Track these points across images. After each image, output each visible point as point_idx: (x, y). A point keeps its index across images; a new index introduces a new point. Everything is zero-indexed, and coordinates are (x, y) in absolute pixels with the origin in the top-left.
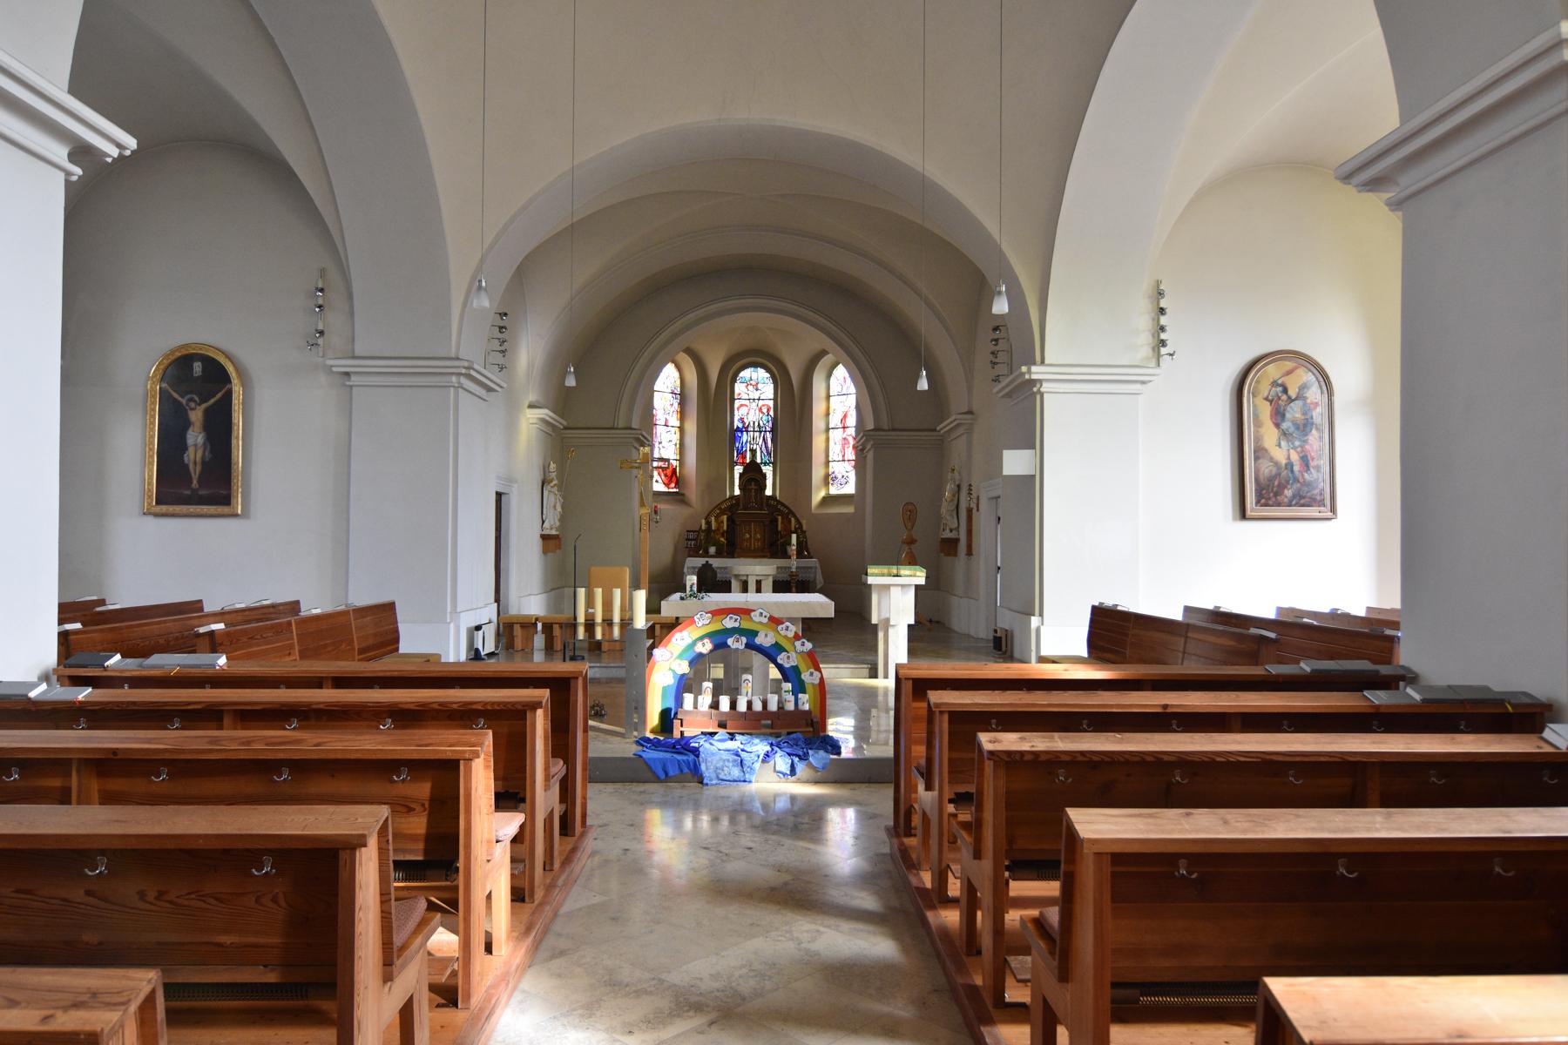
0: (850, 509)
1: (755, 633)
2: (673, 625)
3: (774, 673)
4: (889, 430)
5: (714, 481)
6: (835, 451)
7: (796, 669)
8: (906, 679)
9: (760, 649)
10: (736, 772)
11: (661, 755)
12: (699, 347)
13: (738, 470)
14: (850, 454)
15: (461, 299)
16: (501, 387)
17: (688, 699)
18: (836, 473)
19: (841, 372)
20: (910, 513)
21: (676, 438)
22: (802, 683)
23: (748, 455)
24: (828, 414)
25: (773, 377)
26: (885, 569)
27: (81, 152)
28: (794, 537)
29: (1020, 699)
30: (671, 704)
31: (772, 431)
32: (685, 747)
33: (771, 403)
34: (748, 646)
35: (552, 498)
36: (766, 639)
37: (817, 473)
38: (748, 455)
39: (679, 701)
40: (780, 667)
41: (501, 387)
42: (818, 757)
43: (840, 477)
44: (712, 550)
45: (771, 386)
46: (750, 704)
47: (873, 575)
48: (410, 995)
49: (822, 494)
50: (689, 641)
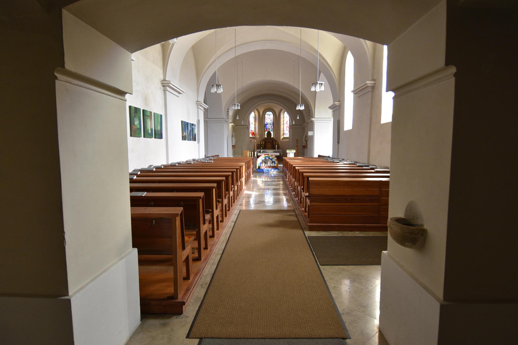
0: (288, 140)
1: (269, 157)
2: (260, 156)
5: (262, 135)
6: (285, 129)
7: (274, 161)
8: (306, 177)
9: (270, 159)
10: (267, 172)
12: (259, 109)
13: (266, 132)
14: (288, 129)
16: (184, 92)
17: (262, 164)
18: (285, 133)
19: (286, 113)
20: (297, 141)
23: (268, 129)
24: (284, 121)
25: (273, 113)
26: (289, 150)
27: (205, 109)
28: (276, 145)
31: (273, 124)
33: (273, 119)
35: (234, 139)
36: (271, 158)
37: (282, 133)
38: (268, 129)
41: (184, 92)
44: (261, 148)
45: (273, 115)
48: (187, 255)
49: (283, 137)
50: (261, 158)
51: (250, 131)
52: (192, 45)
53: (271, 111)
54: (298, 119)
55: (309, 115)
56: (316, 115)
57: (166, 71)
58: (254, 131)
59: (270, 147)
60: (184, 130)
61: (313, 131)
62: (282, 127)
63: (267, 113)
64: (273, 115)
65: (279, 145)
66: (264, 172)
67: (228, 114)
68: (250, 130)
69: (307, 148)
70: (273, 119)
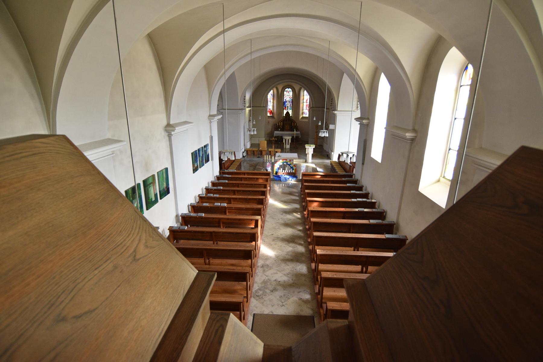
0: (307, 120)
3: (290, 167)
7: (293, 167)
10: (285, 180)
11: (276, 178)
14: (308, 108)
15: (240, 96)
17: (279, 170)
19: (305, 91)
21: (272, 104)
24: (303, 99)
29: (244, 231)
31: (292, 102)
32: (279, 177)
33: (292, 96)
36: (289, 163)
37: (301, 112)
42: (294, 179)
44: (279, 130)
47: (306, 146)
49: (302, 116)
52: (204, 65)
53: (290, 88)
55: (331, 104)
56: (339, 108)
58: (272, 110)
59: (288, 129)
60: (195, 160)
61: (334, 124)
62: (301, 105)
63: (286, 90)
64: (293, 92)
65: (298, 126)
66: (281, 181)
67: (245, 102)
68: (268, 108)
70: (293, 96)
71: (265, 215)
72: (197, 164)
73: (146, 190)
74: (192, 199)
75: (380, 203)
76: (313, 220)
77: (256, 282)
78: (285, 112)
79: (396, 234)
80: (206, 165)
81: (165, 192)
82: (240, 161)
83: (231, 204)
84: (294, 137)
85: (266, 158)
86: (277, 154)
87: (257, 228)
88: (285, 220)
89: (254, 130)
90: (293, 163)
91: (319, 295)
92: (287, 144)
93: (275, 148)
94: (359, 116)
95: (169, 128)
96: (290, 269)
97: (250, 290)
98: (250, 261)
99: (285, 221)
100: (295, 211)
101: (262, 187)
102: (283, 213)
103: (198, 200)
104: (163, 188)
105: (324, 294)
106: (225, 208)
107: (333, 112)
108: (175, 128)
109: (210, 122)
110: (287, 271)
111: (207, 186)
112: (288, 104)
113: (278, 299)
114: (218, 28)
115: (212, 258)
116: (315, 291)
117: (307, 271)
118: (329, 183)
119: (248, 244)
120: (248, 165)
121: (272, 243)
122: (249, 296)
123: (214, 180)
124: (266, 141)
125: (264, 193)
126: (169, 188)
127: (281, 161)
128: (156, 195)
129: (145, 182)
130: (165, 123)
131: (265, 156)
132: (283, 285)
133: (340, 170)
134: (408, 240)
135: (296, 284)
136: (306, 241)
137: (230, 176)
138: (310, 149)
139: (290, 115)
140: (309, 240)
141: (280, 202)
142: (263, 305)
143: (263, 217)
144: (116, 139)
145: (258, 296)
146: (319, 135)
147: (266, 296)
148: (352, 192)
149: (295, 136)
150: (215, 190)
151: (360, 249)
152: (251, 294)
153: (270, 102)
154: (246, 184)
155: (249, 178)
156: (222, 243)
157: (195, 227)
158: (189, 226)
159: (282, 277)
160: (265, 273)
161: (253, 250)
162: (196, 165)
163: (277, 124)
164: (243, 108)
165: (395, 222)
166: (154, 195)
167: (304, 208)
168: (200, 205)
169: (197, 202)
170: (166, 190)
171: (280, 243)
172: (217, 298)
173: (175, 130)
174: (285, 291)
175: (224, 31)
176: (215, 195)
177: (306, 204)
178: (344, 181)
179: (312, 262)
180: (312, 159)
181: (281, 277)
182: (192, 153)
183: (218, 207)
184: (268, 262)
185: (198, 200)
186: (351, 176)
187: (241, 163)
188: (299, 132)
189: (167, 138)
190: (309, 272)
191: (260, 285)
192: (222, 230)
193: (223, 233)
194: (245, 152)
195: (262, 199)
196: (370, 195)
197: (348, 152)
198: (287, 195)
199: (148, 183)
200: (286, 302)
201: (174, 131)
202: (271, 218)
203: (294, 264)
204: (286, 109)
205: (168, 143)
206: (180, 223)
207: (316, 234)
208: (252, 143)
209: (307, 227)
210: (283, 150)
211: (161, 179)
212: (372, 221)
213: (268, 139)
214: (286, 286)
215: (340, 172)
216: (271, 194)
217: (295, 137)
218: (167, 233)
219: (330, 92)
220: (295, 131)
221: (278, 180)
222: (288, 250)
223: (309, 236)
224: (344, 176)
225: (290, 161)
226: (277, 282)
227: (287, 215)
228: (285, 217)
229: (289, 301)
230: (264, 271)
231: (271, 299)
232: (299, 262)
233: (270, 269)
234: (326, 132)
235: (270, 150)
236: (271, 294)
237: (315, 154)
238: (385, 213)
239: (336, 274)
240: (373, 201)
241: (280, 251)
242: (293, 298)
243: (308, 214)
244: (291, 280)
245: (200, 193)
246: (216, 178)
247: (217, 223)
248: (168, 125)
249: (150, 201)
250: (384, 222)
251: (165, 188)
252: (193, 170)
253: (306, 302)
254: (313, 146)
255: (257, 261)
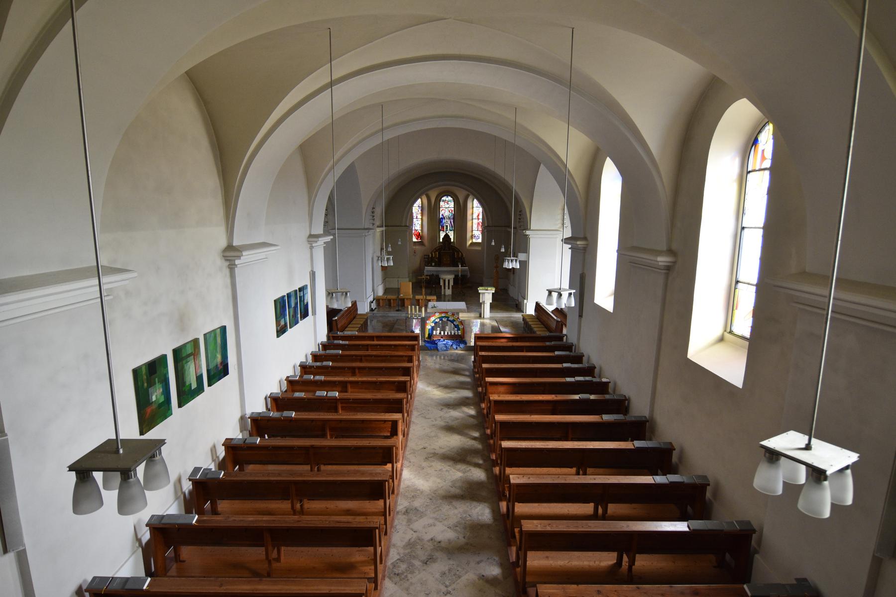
0: (479, 248)
1: (449, 317)
4: (492, 227)
7: (458, 325)
9: (450, 321)
10: (445, 348)
19: (475, 201)
21: (420, 222)
22: (459, 328)
24: (473, 214)
26: (483, 288)
29: (370, 443)
30: (430, 332)
31: (453, 219)
33: (453, 209)
34: (447, 320)
36: (451, 319)
37: (469, 235)
39: (432, 332)
40: (454, 324)
42: (462, 346)
43: (476, 236)
44: (433, 264)
45: (453, 203)
46: (448, 333)
47: (480, 290)
49: (471, 242)
50: (434, 319)
51: (413, 231)
54: (503, 252)
55: (520, 219)
56: (534, 225)
57: (233, 227)
62: (469, 224)
63: (443, 199)
66: (438, 350)
68: (413, 229)
69: (515, 272)
71: (409, 413)
72: (285, 320)
73: (179, 368)
74: (274, 386)
75: (615, 384)
76: (499, 417)
77: (394, 545)
78: (442, 235)
79: (650, 440)
80: (302, 323)
81: (219, 372)
82: (366, 317)
83: (346, 392)
84: (458, 276)
85: (412, 310)
86: (431, 304)
87: (395, 437)
88: (446, 421)
89: (388, 259)
90: (458, 318)
91: (518, 567)
92: (447, 287)
93: (426, 294)
94: (570, 236)
95: (231, 253)
96: (459, 516)
97: (381, 563)
98: (381, 502)
99: (448, 422)
100: (464, 402)
101: (404, 361)
102: (442, 407)
103: (284, 387)
104: (215, 365)
105: (529, 563)
106: (335, 399)
107: (524, 231)
108: (242, 252)
109: (311, 248)
110: (453, 520)
111: (304, 360)
112: (447, 223)
113: (437, 579)
114: (320, 78)
115: (308, 500)
116: (508, 559)
117: (492, 518)
118: (523, 352)
119: (378, 469)
120: (380, 324)
121: (424, 464)
122: (380, 576)
123: (318, 350)
124: (411, 283)
125: (407, 372)
126: (227, 364)
127: (437, 315)
128: (199, 378)
129: (176, 352)
130: (223, 243)
131: (409, 307)
132: (447, 549)
133: (540, 329)
134: (675, 449)
135: (471, 545)
136: (487, 459)
137: (347, 342)
138: (487, 295)
139: (451, 239)
140: (494, 457)
141: (437, 388)
142: (408, 594)
143: (406, 415)
144: (119, 266)
145: (398, 575)
146: (504, 267)
147: (415, 574)
148: (565, 365)
149: (460, 274)
150: (318, 367)
151: (589, 470)
152: (384, 571)
153: (417, 218)
154: (375, 356)
155: (380, 345)
156: (329, 468)
157: (279, 438)
158: (266, 437)
159: (444, 533)
160: (411, 526)
161: (386, 481)
162: (282, 323)
163: (429, 255)
164: (371, 226)
165: (647, 417)
166: (196, 377)
167: (481, 397)
168: (289, 395)
169: (284, 390)
170: (221, 367)
171: (440, 463)
172: (312, 588)
173: (242, 255)
174: (451, 562)
175: (331, 84)
176: (318, 378)
177: (484, 389)
178: (549, 346)
179: (501, 500)
180: (490, 312)
181: (443, 532)
182: (275, 301)
183: (321, 400)
184: (417, 504)
185: (286, 388)
186: (560, 338)
187: (367, 320)
188: (467, 268)
189: (227, 272)
190: (495, 519)
191: (402, 551)
192: (330, 442)
193: (331, 448)
194: (374, 302)
195: (405, 382)
196: (597, 371)
197: (560, 289)
198: (449, 375)
199: (184, 355)
200: (453, 586)
201: (239, 257)
202: (422, 417)
203: (468, 504)
204: (443, 231)
205: (228, 281)
206: (248, 432)
207: (506, 444)
208: (387, 287)
209: (488, 431)
210: (440, 299)
211: (211, 347)
212: (606, 417)
213: (414, 280)
214: (452, 550)
215: (540, 331)
216: (421, 373)
217: (460, 276)
218: (222, 452)
219: (518, 202)
220: (460, 266)
221: (432, 348)
222: (454, 478)
223: (491, 449)
224: (549, 339)
225: (453, 315)
226: (436, 543)
227: (450, 410)
228: (447, 415)
229: (458, 583)
230: (409, 521)
231: (424, 579)
232: (476, 501)
233: (421, 517)
234: (516, 261)
235: (417, 297)
236: (424, 570)
237: (495, 303)
238: (627, 402)
239: (550, 524)
240: (604, 380)
241: (439, 480)
242: (467, 574)
243: (489, 408)
244: (461, 537)
245: (290, 373)
246: (321, 346)
247: (318, 429)
248: (230, 248)
249: (186, 389)
250: (628, 418)
251: (219, 366)
252: (277, 332)
253: (492, 582)
254: (492, 290)
255: (396, 502)
